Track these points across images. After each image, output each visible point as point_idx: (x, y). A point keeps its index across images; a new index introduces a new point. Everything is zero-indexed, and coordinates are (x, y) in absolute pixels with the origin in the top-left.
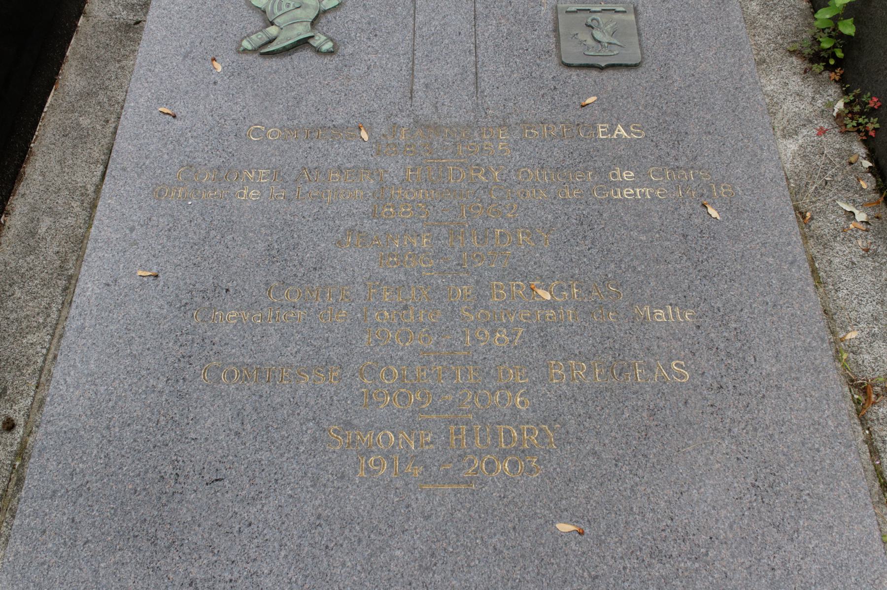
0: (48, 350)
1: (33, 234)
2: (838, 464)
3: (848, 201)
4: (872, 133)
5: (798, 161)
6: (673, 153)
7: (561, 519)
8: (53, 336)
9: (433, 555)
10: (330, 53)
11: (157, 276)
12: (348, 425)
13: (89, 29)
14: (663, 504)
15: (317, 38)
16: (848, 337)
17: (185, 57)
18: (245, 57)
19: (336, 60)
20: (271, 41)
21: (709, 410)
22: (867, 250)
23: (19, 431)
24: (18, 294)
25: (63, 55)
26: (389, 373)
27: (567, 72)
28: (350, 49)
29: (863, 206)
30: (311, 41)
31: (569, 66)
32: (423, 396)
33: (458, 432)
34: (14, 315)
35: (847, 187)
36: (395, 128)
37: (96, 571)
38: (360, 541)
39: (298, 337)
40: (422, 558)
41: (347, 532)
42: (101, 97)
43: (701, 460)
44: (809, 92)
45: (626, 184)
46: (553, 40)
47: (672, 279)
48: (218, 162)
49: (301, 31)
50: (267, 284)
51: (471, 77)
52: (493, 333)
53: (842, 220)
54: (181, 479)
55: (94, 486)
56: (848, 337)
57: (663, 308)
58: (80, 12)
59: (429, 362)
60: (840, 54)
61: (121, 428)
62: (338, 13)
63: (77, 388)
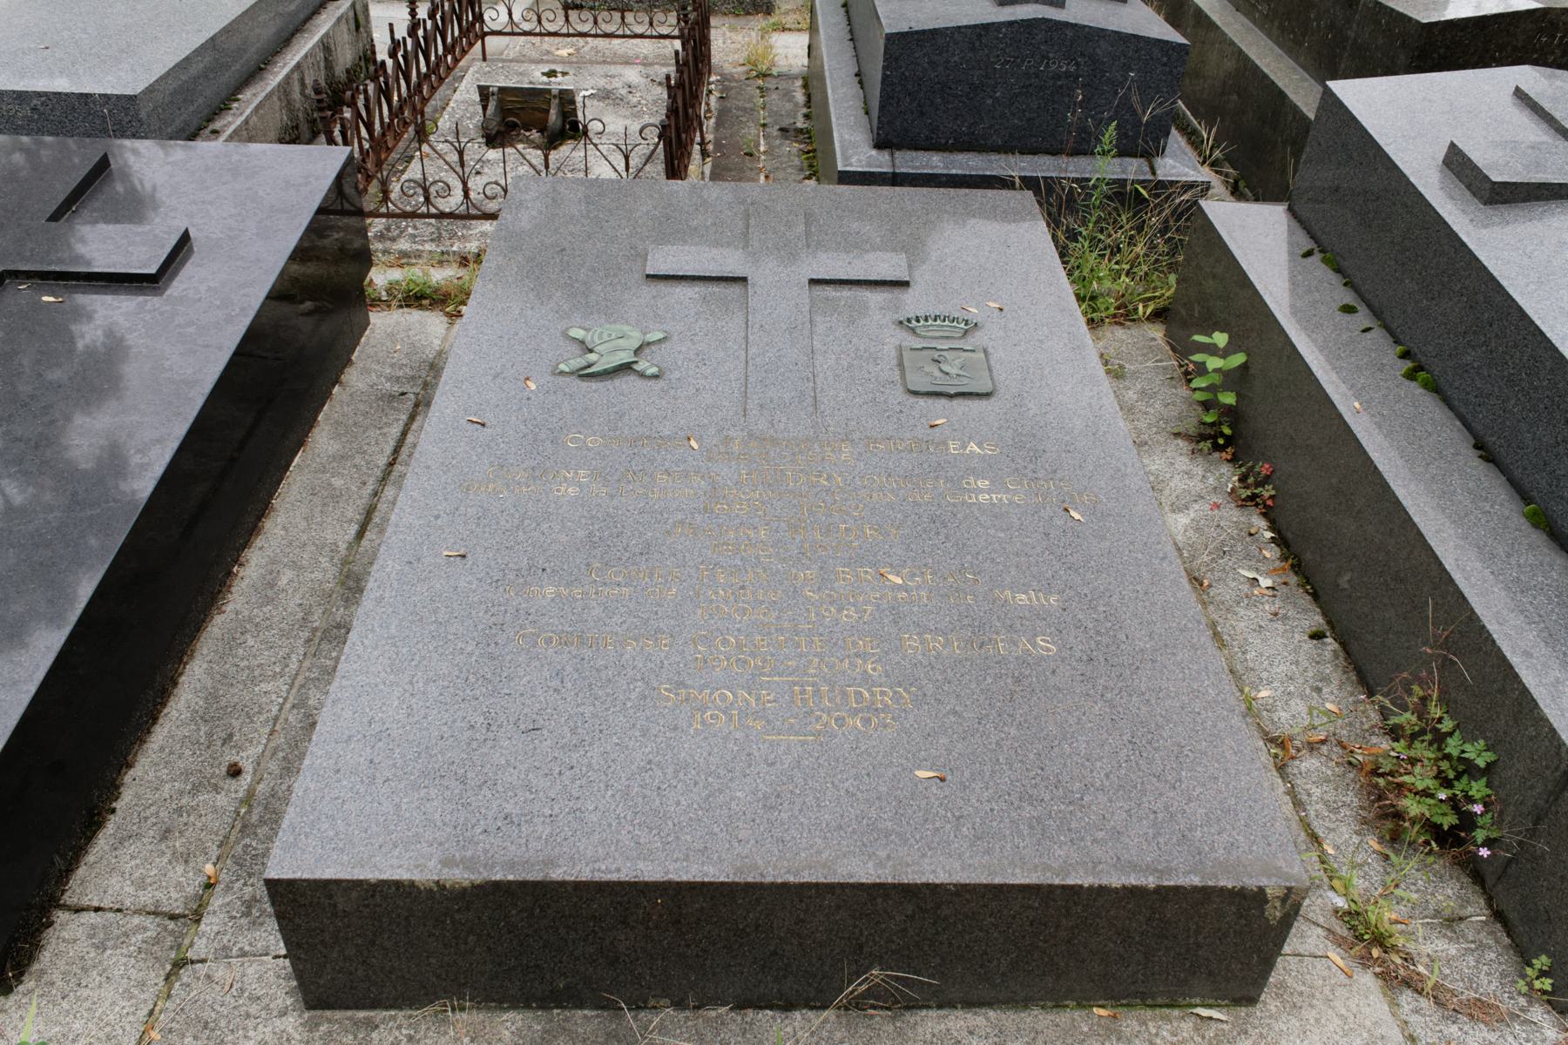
0: (286, 699)
1: (271, 585)
2: (1221, 725)
3: (1250, 568)
4: (1269, 502)
5: (1190, 533)
6: (1031, 466)
7: (919, 768)
8: (292, 686)
9: (778, 796)
10: (656, 377)
11: (464, 556)
12: (682, 684)
13: (345, 397)
14: (1032, 756)
16: (1262, 694)
17: (496, 376)
18: (561, 379)
19: (661, 383)
20: (589, 366)
21: (1079, 678)
22: (1276, 614)
23: (246, 779)
24: (251, 642)
25: (315, 419)
26: (725, 642)
27: (913, 399)
28: (677, 374)
29: (1268, 574)
30: (635, 367)
31: (915, 393)
32: (764, 661)
33: (803, 692)
34: (245, 663)
35: (1248, 557)
36: (727, 440)
37: (398, 806)
38: (696, 784)
39: (623, 610)
40: (765, 798)
41: (681, 775)
42: (358, 460)
43: (1072, 720)
44: (1199, 471)
45: (982, 491)
46: (897, 372)
47: (1034, 569)
48: (533, 463)
49: (625, 357)
50: (588, 565)
51: (810, 400)
52: (840, 610)
53: (1245, 588)
54: (494, 728)
55: (395, 733)
56: (1262, 694)
57: (1025, 593)
58: (337, 381)
59: (769, 633)
60: (1227, 431)
61: (426, 683)
63: (376, 648)
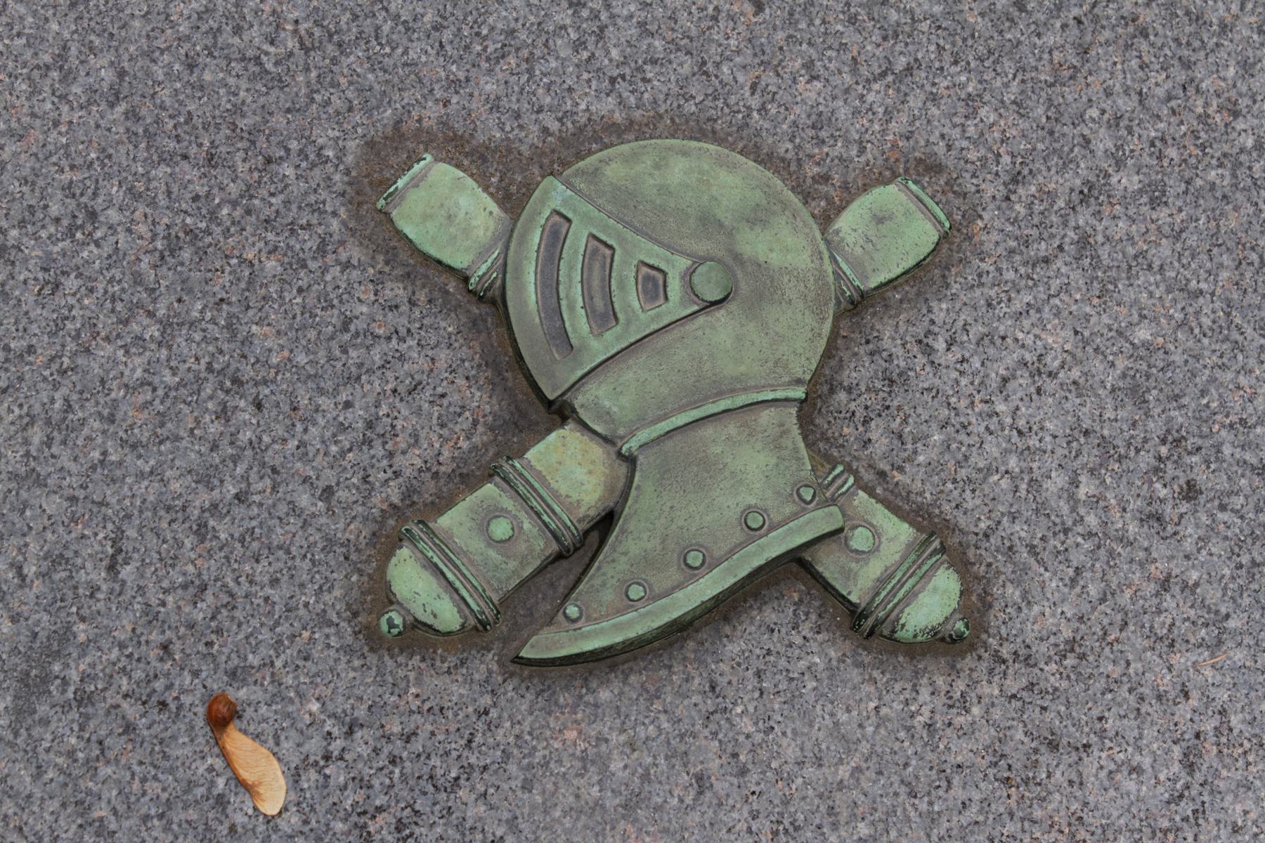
10: (946, 645)
15: (860, 539)
62: (941, 310)
